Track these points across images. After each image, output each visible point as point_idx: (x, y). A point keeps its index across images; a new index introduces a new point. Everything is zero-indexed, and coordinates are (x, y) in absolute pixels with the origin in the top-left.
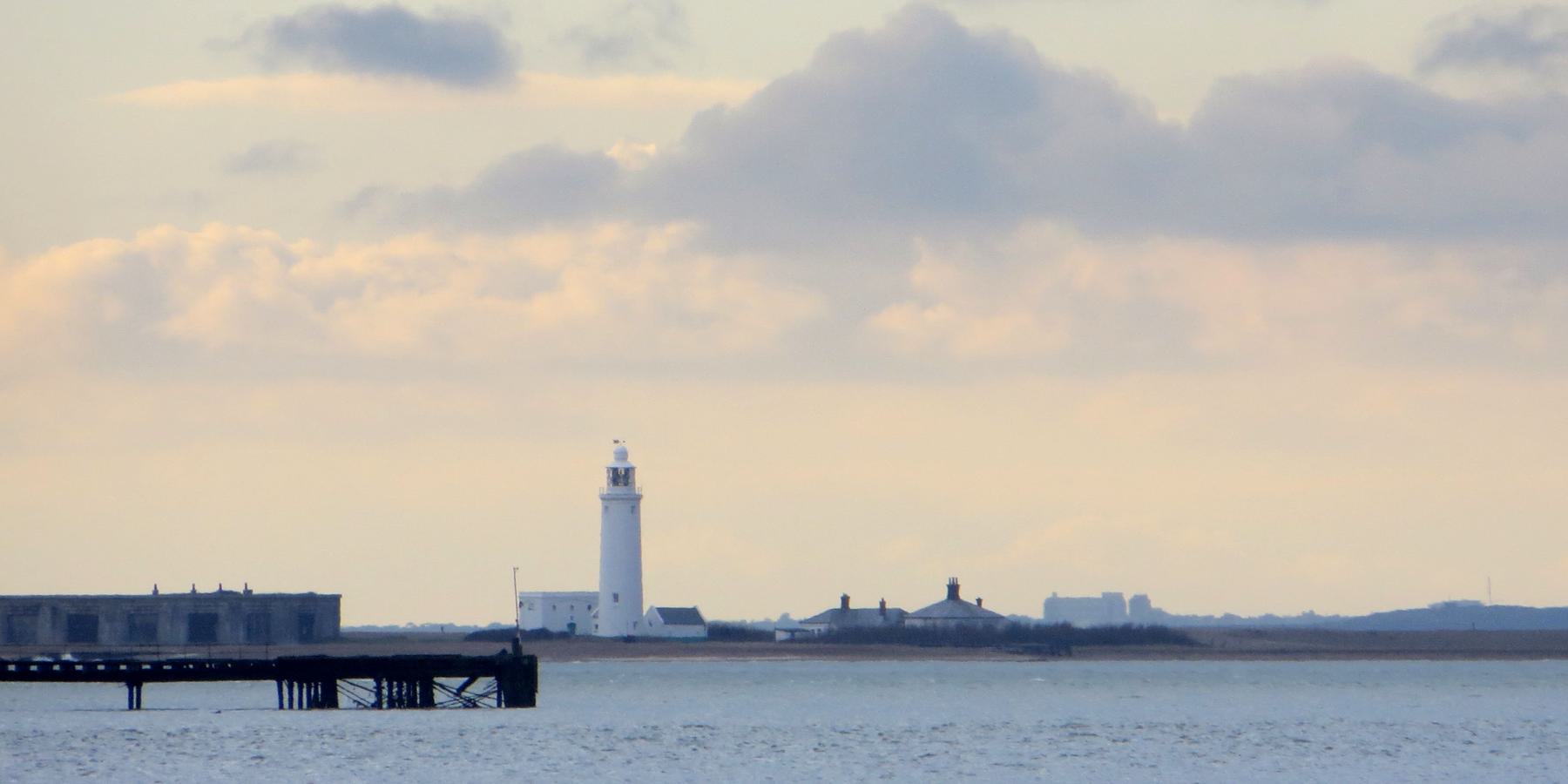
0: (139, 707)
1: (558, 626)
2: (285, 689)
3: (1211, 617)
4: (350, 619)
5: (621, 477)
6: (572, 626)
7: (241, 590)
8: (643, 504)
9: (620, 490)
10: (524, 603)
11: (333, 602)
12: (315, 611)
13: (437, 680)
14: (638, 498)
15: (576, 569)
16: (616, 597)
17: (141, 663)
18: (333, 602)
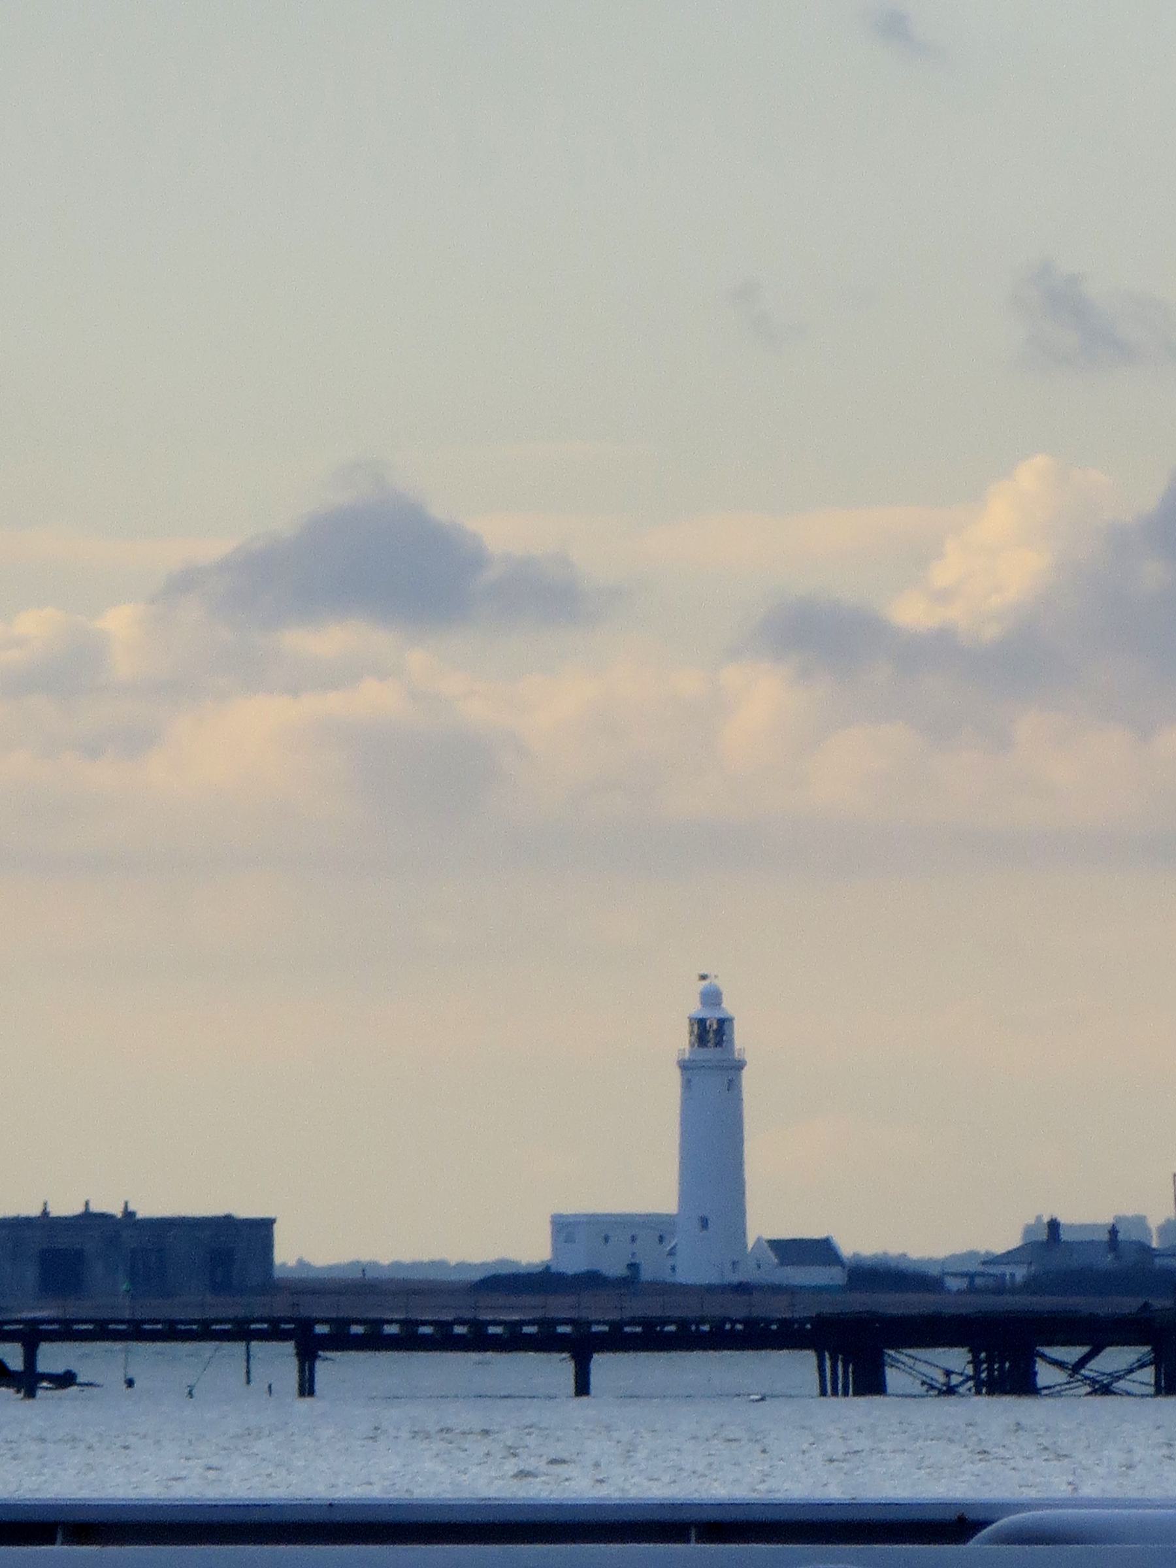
0: (311, 1393)
1: (614, 1268)
2: (828, 1364)
3: (374, 1265)
4: (288, 1252)
5: (711, 1032)
6: (634, 1267)
7: (117, 1211)
8: (746, 1074)
9: (710, 1053)
10: (565, 1229)
11: (263, 1227)
12: (234, 1246)
13: (320, 1353)
14: (739, 1066)
15: (644, 1180)
16: (704, 1223)
17: (590, 1323)
18: (263, 1227)
